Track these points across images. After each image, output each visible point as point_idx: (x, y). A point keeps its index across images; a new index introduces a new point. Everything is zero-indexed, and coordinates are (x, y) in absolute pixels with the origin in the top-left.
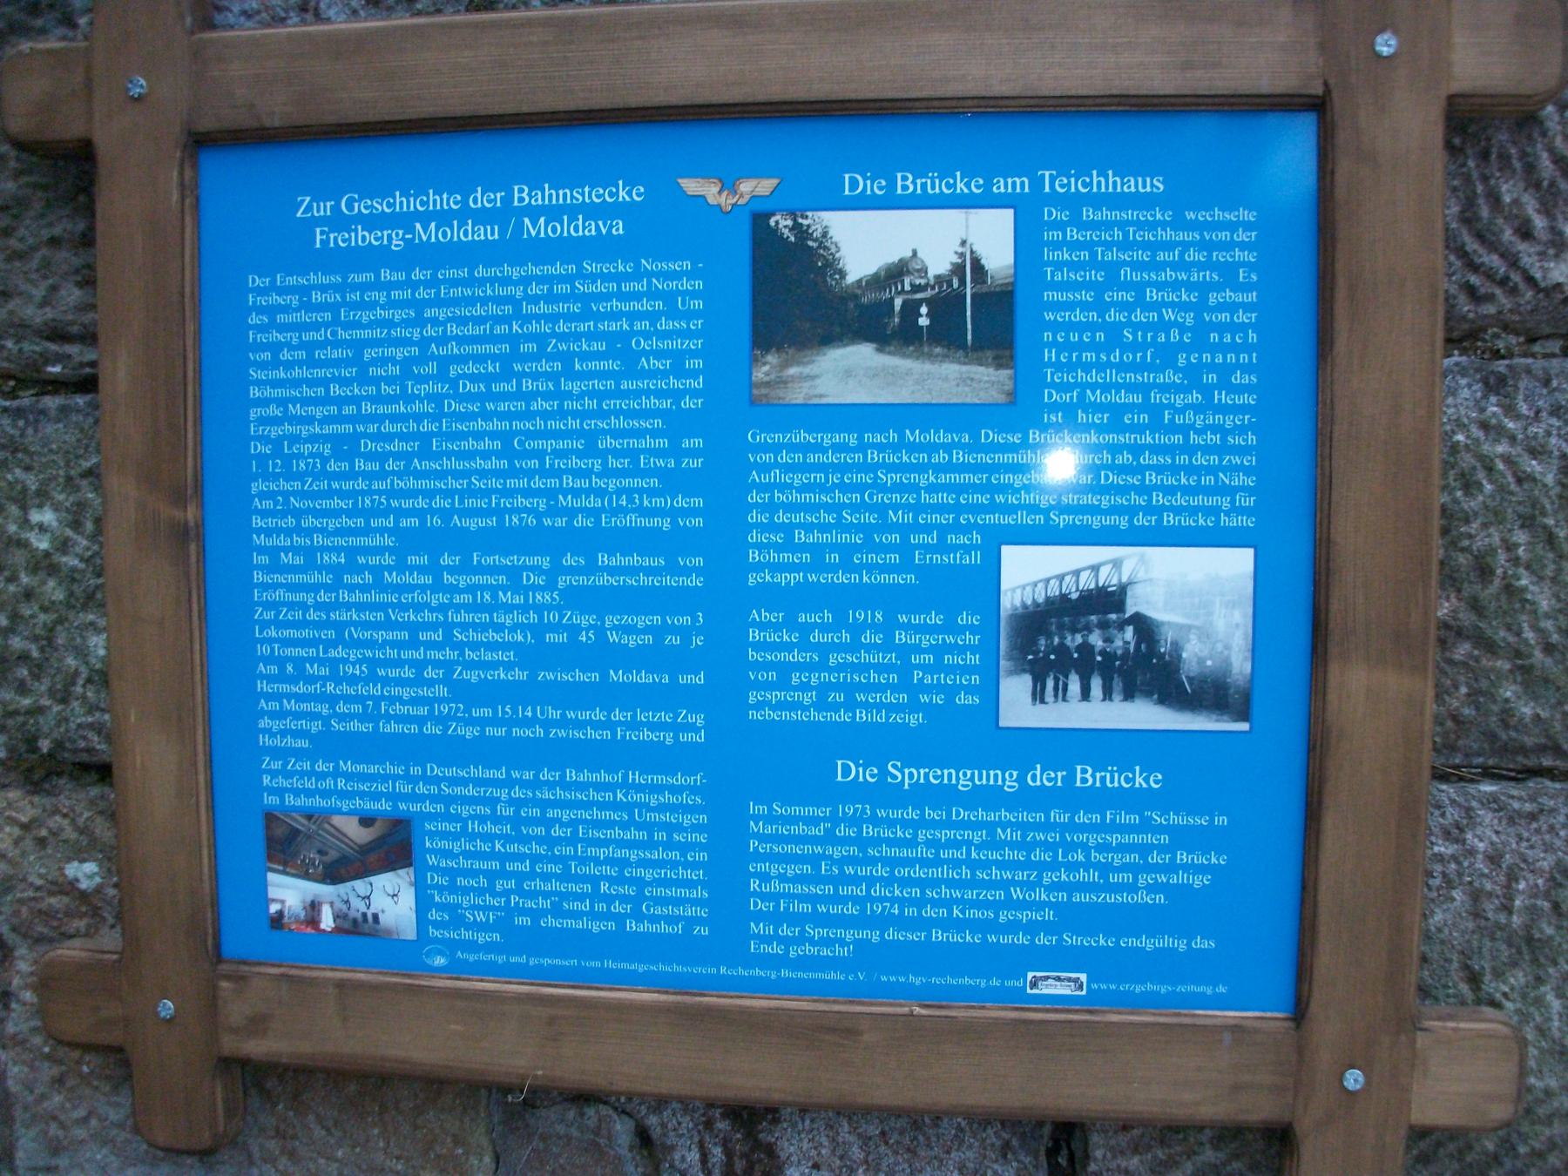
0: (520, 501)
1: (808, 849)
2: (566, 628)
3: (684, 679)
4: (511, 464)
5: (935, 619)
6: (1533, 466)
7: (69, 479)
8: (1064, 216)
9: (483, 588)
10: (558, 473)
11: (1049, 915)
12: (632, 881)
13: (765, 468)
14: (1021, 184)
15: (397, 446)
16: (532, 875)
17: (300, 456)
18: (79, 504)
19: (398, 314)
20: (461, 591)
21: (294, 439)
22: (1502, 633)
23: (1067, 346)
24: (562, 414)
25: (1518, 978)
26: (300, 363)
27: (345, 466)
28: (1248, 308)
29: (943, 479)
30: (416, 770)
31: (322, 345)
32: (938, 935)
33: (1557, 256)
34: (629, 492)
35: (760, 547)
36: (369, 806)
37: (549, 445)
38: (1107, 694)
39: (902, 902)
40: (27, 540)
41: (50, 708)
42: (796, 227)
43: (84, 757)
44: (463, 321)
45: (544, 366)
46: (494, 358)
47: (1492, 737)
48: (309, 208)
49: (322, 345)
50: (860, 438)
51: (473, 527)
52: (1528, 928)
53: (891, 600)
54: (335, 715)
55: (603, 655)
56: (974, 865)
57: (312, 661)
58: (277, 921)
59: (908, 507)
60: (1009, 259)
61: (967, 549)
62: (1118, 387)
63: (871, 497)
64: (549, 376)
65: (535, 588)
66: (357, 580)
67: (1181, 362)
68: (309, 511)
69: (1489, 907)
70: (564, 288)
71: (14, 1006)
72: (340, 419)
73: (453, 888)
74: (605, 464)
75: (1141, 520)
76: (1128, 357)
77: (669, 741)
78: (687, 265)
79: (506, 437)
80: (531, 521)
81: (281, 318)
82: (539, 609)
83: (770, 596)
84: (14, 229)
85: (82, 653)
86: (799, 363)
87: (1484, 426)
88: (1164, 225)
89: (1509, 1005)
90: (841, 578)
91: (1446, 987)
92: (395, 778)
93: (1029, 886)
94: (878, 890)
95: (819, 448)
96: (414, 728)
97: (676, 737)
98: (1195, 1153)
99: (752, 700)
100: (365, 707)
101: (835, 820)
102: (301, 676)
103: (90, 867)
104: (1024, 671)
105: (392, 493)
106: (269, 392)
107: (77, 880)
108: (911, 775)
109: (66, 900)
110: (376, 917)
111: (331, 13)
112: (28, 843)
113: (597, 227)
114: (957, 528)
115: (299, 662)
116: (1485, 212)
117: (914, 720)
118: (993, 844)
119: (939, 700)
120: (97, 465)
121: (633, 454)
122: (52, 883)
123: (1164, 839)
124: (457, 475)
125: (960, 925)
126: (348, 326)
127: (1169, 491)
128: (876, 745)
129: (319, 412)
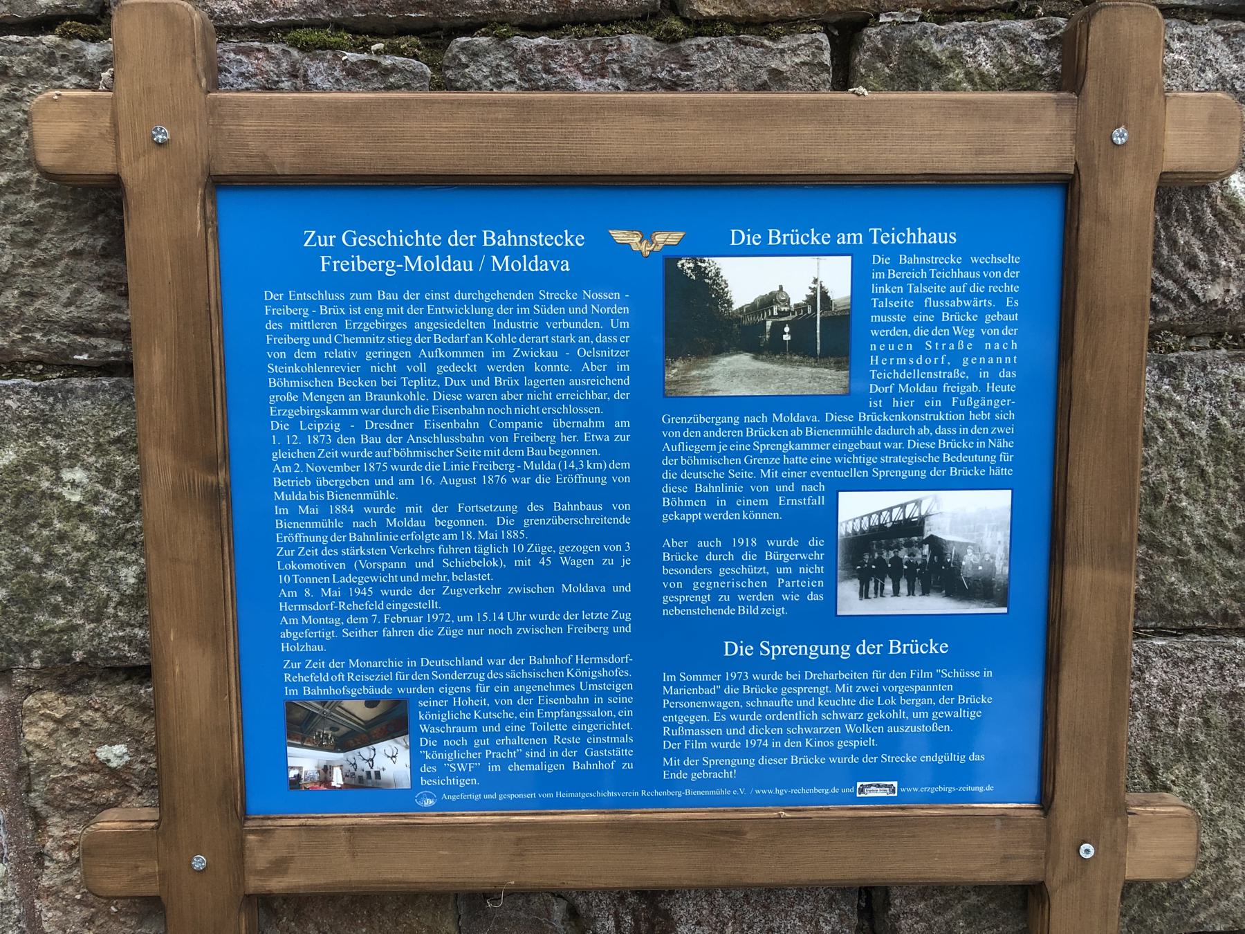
0: (494, 466)
1: (704, 704)
2: (529, 556)
3: (616, 589)
4: (487, 439)
5: (793, 543)
6: (1192, 425)
7: (99, 446)
8: (887, 261)
9: (466, 529)
10: (523, 446)
11: (872, 742)
12: (577, 734)
13: (675, 441)
14: (857, 238)
15: (396, 425)
16: (502, 734)
17: (314, 432)
18: (108, 465)
19: (394, 326)
20: (449, 532)
21: (308, 419)
22: (1169, 539)
23: (887, 354)
24: (525, 403)
25: (1181, 770)
26: (312, 362)
27: (352, 440)
28: (1011, 325)
29: (799, 447)
30: (412, 663)
31: (330, 347)
32: (795, 760)
33: (1213, 280)
34: (577, 459)
35: (670, 495)
36: (373, 691)
37: (516, 425)
38: (911, 592)
39: (770, 738)
40: (60, 494)
41: (83, 625)
42: (697, 269)
43: (116, 663)
44: (445, 333)
45: (512, 368)
46: (472, 361)
47: (1161, 608)
48: (315, 240)
49: (330, 347)
50: (741, 420)
51: (458, 485)
52: (1188, 736)
53: (763, 531)
54: (346, 626)
55: (557, 574)
56: (819, 710)
57: (326, 586)
58: (296, 783)
59: (773, 467)
60: (846, 292)
61: (815, 495)
62: (921, 381)
63: (748, 460)
64: (514, 375)
65: (506, 528)
66: (363, 525)
67: (965, 363)
68: (322, 474)
69: (1161, 722)
70: (526, 310)
71: (47, 864)
72: (347, 405)
73: (440, 748)
74: (558, 438)
75: (935, 473)
76: (928, 361)
77: (606, 632)
78: (617, 295)
79: (483, 419)
80: (503, 480)
81: (294, 326)
82: (509, 543)
83: (678, 530)
84: (37, 241)
85: (114, 582)
86: (698, 368)
87: (1160, 399)
88: (955, 267)
89: (1175, 788)
90: (728, 516)
91: (1133, 778)
92: (395, 670)
93: (859, 723)
94: (754, 730)
95: (712, 427)
96: (411, 633)
97: (611, 630)
98: (964, 898)
99: (665, 602)
100: (371, 619)
101: (723, 683)
102: (317, 597)
103: (120, 749)
104: (854, 577)
105: (392, 461)
106: (285, 383)
107: (109, 761)
108: (776, 650)
109: (97, 776)
110: (378, 774)
111: (318, 80)
112: (62, 733)
113: (549, 265)
114: (808, 481)
115: (315, 588)
116: (1165, 251)
117: (779, 612)
118: (833, 695)
119: (795, 598)
120: (124, 435)
121: (579, 432)
122: (84, 764)
123: (950, 687)
124: (444, 447)
125: (810, 752)
126: (351, 333)
127: (955, 452)
128: (751, 630)
129: (330, 399)
